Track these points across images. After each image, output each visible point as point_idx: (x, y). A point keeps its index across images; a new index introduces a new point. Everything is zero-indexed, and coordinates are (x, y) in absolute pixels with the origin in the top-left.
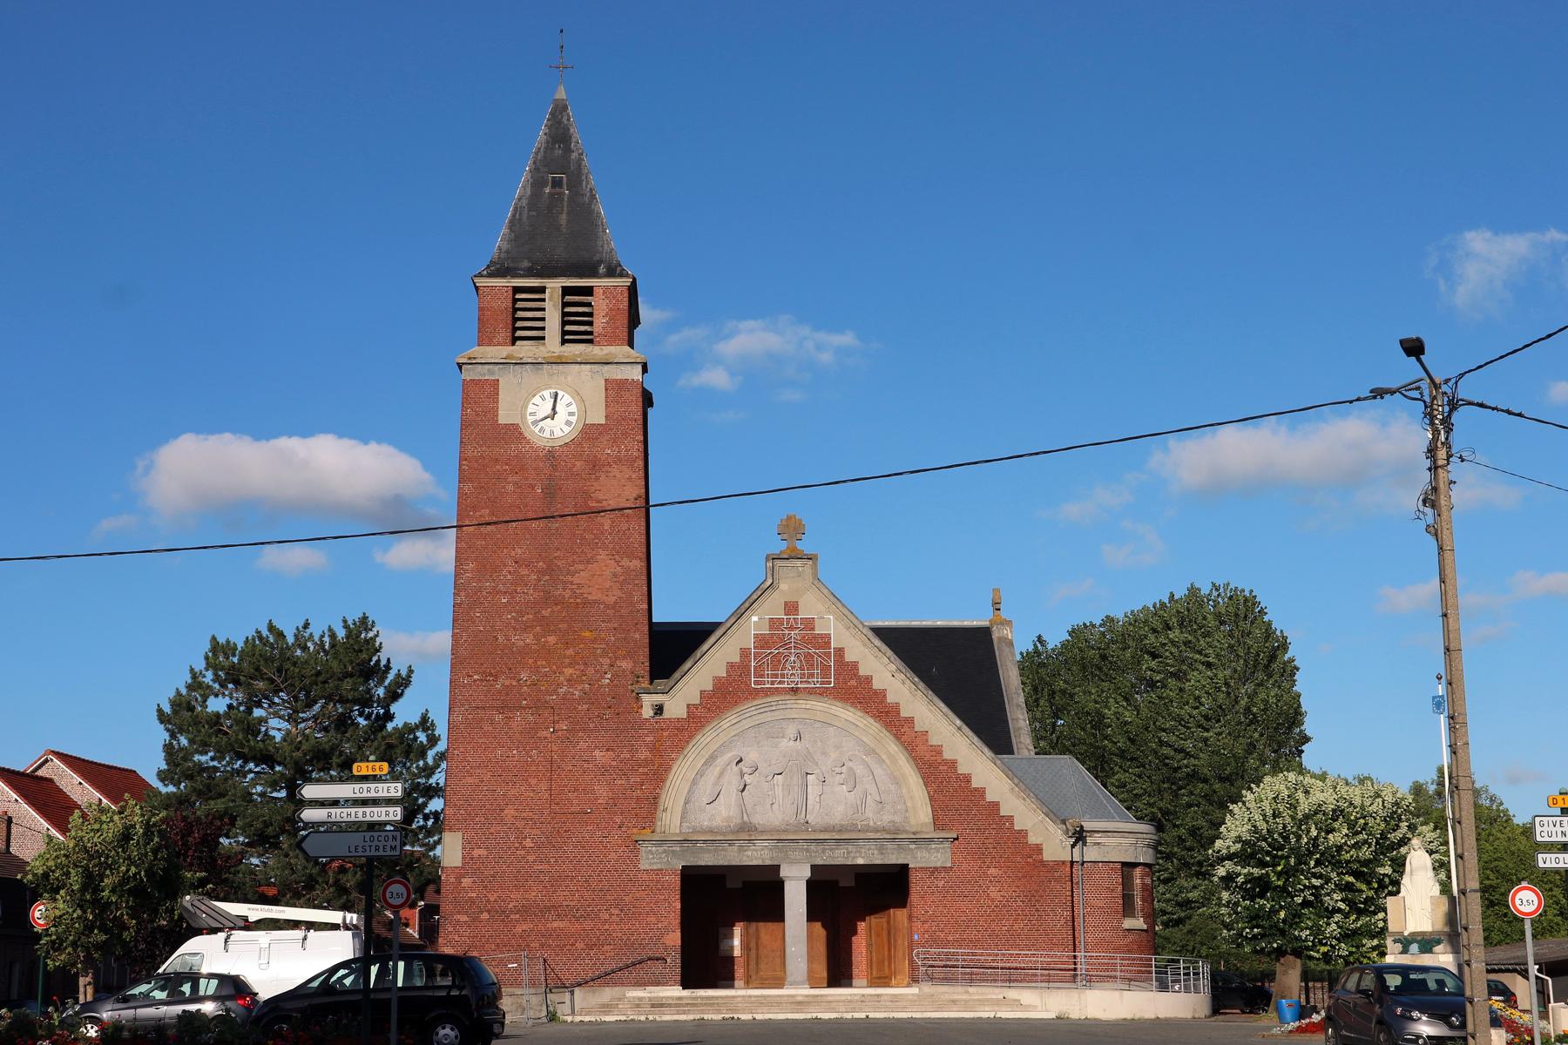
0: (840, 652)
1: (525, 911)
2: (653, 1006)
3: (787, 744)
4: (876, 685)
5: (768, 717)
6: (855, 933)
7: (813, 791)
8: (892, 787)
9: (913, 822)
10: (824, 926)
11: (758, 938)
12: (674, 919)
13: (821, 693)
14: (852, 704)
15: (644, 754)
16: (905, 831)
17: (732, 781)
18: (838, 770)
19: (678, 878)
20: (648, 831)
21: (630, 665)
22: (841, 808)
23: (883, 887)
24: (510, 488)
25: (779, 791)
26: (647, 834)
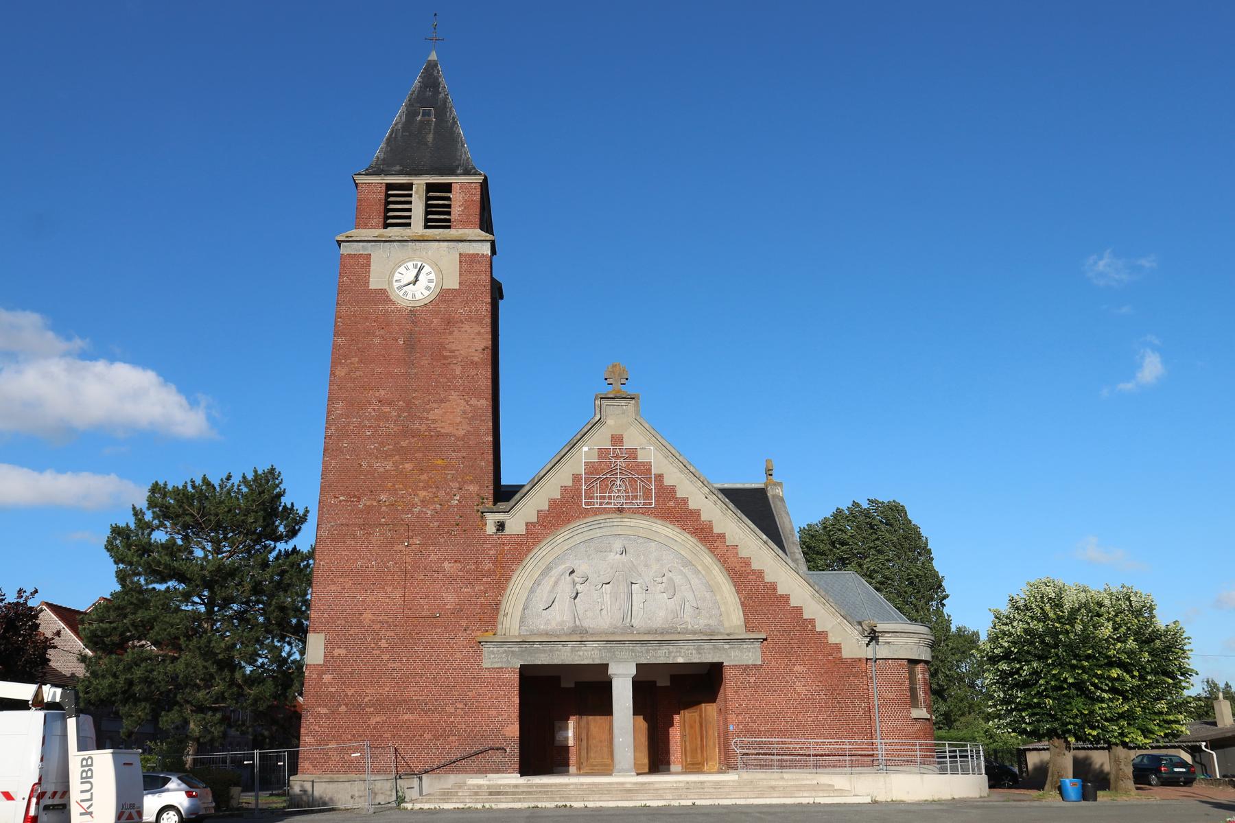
0: (660, 477)
1: (379, 705)
2: (491, 794)
3: (614, 557)
5: (598, 533)
7: (638, 598)
8: (708, 595)
9: (726, 624)
13: (644, 512)
14: (671, 522)
15: (488, 566)
17: (565, 589)
18: (659, 580)
19: (517, 676)
20: (490, 634)
22: (662, 614)
23: (700, 683)
24: (377, 340)
25: (607, 598)
26: (489, 636)
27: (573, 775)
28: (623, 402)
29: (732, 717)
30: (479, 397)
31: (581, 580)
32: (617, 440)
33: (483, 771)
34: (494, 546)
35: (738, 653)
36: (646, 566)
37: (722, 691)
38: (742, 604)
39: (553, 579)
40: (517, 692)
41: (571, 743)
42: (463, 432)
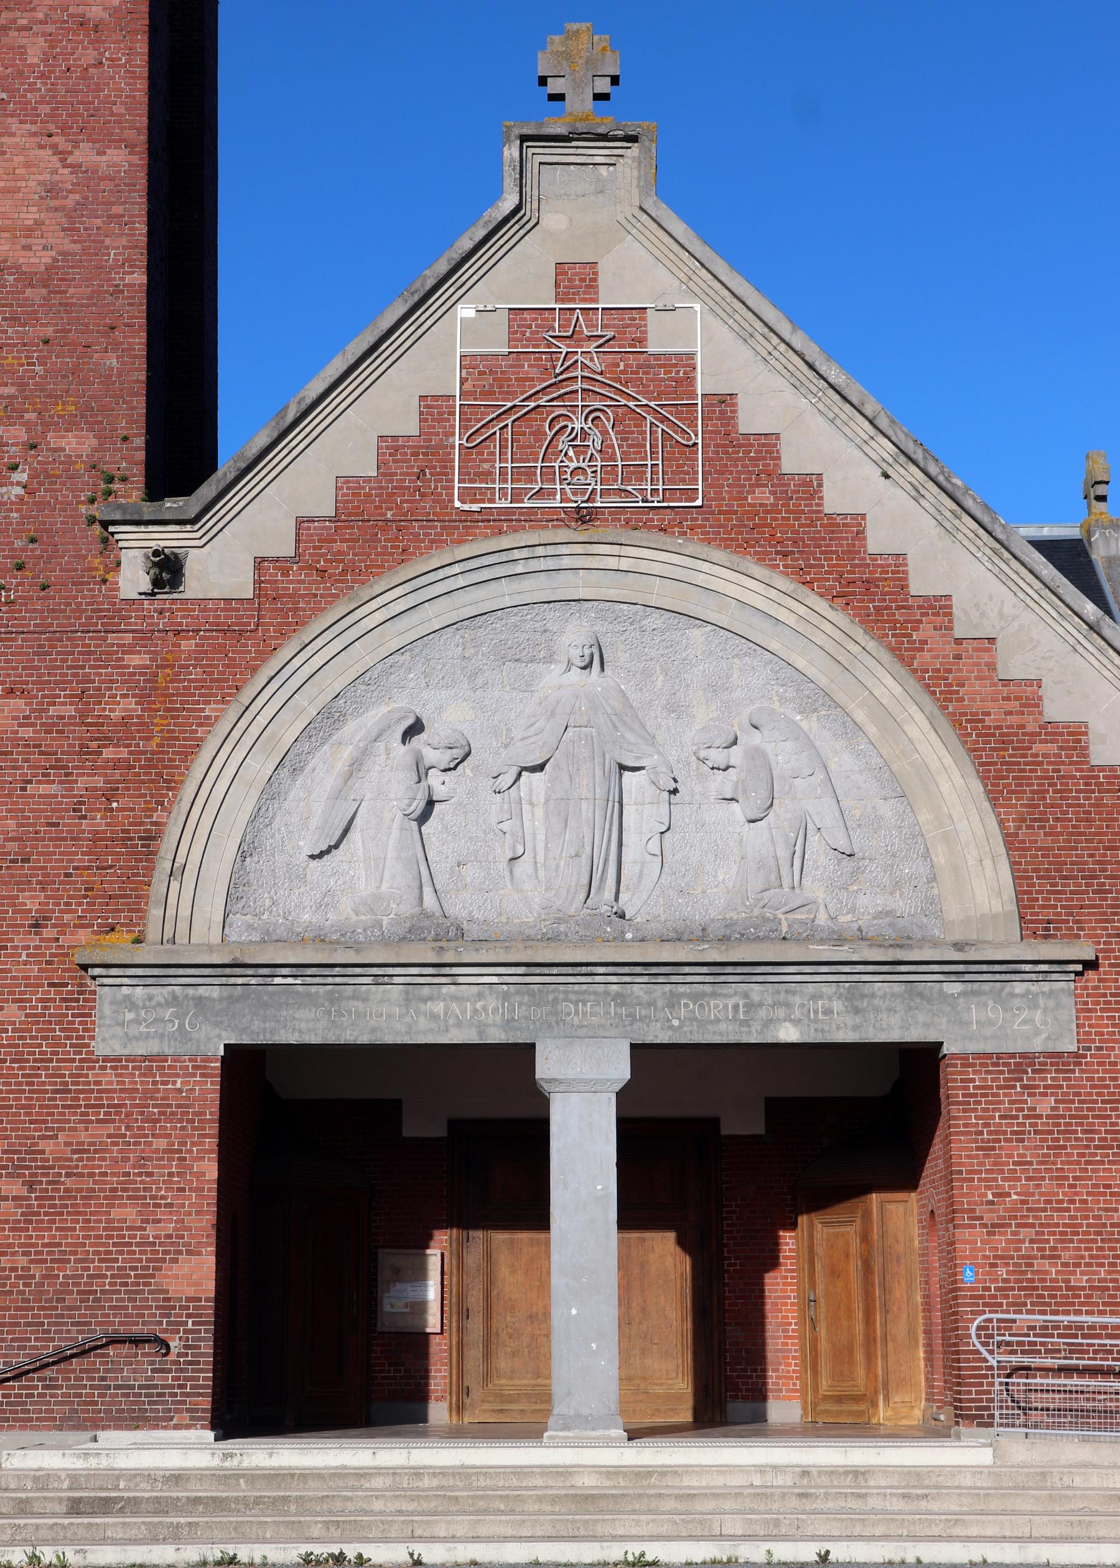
0: (723, 405)
2: (76, 1507)
3: (559, 681)
4: (834, 501)
5: (505, 594)
6: (772, 1262)
7: (643, 814)
8: (887, 810)
9: (953, 911)
10: (682, 1242)
11: (490, 1280)
12: (198, 1215)
13: (667, 521)
14: (761, 558)
15: (122, 706)
16: (936, 944)
17: (389, 786)
18: (717, 757)
19: (211, 1088)
20: (124, 937)
21: (91, 442)
22: (727, 874)
23: (866, 1119)
25: (535, 821)
26: (118, 948)
27: (787, 1433)
28: (599, 153)
29: (971, 1239)
30: (104, 140)
31: (444, 758)
32: (576, 279)
33: (88, 1418)
34: (144, 637)
35: (992, 1012)
36: (675, 708)
37: (937, 1148)
38: (1011, 841)
39: (347, 753)
40: (211, 1143)
41: (433, 1323)
42: (46, 258)
